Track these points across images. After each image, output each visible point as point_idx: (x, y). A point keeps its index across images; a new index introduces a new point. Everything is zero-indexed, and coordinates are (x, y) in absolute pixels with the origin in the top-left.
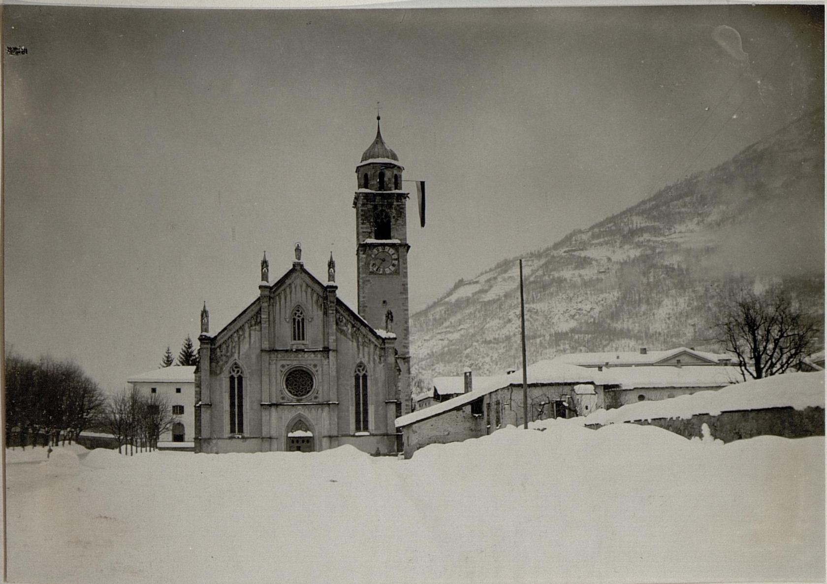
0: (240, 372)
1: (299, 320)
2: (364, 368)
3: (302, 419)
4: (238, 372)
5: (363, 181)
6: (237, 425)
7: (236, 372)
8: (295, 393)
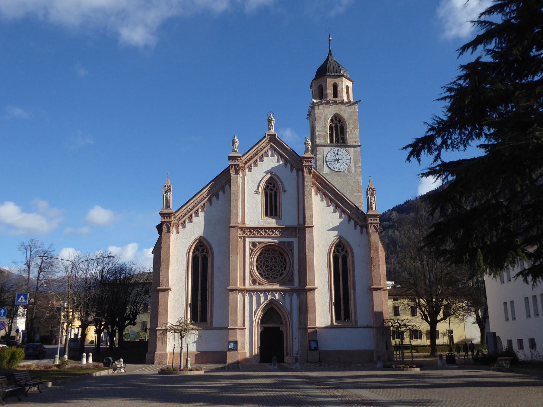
1: (271, 193)
3: (274, 307)
5: (317, 93)
6: (161, 385)
8: (267, 276)
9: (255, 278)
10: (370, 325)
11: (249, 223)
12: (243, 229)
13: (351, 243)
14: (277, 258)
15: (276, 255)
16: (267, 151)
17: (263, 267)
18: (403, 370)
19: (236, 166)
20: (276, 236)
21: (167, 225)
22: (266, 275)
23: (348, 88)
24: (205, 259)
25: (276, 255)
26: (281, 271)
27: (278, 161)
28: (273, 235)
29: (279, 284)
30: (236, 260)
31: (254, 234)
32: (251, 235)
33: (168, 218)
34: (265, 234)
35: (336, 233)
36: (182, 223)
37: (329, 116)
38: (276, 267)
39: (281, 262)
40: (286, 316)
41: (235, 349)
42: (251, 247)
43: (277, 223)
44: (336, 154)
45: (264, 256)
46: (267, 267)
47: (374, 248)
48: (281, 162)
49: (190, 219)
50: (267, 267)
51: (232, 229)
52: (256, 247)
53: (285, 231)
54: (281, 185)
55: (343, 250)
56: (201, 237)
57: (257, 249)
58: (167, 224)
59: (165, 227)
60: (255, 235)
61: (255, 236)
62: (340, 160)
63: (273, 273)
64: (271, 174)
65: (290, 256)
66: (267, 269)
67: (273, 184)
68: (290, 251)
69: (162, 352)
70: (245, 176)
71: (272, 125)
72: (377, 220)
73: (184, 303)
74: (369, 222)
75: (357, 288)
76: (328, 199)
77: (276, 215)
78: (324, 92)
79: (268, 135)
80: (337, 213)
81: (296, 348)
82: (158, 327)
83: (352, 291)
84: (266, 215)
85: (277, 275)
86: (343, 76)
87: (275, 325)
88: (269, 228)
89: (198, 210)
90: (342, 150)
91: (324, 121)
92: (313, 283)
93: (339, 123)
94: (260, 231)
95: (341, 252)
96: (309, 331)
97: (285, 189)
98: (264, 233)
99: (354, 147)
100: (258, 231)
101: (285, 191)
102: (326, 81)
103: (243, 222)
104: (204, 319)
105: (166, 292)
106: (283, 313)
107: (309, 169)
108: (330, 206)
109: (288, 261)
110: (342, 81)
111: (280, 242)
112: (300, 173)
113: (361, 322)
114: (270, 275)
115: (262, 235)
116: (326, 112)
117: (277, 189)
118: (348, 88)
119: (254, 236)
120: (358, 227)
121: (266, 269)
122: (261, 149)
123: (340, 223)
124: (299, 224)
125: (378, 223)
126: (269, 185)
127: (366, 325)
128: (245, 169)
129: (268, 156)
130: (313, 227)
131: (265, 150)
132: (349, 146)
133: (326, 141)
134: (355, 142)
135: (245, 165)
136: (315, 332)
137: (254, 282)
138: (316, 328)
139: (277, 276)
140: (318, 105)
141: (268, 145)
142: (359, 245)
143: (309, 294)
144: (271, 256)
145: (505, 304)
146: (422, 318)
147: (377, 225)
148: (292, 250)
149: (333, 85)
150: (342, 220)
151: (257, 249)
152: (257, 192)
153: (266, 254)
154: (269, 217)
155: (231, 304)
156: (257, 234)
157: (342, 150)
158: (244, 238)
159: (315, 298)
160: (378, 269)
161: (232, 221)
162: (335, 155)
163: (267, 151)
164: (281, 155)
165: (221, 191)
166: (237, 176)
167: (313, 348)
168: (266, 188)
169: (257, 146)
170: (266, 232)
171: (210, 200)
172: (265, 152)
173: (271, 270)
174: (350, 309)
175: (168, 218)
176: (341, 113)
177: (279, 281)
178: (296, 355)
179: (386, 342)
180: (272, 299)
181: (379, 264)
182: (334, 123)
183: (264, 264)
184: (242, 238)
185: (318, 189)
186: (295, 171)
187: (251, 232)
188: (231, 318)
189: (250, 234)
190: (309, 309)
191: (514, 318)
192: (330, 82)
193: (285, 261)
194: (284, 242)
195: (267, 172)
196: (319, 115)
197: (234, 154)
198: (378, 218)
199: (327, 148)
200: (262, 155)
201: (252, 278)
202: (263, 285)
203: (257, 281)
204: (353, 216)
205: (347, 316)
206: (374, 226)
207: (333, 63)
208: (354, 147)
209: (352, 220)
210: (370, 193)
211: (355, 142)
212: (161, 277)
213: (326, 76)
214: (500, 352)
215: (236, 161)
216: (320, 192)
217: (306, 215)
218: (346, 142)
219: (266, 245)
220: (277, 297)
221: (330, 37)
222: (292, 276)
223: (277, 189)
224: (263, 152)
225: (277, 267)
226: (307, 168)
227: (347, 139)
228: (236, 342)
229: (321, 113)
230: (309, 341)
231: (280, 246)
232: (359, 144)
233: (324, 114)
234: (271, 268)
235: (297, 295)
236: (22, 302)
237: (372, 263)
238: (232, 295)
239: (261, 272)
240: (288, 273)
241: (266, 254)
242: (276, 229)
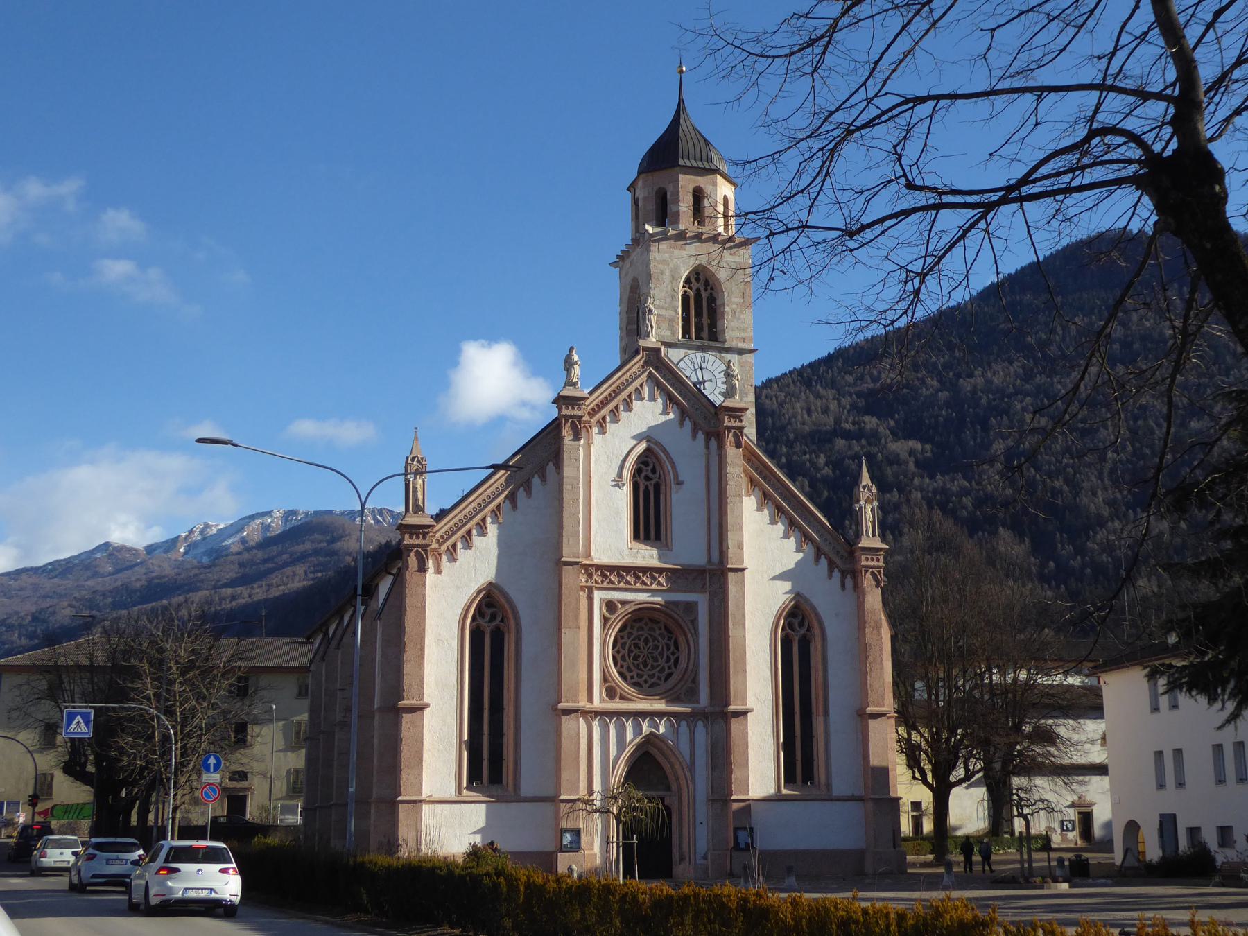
0: (499, 618)
1: (647, 487)
2: (803, 619)
3: (653, 751)
4: (493, 617)
5: (652, 206)
7: (488, 618)
8: (636, 679)
9: (613, 685)
10: (857, 794)
12: (589, 569)
13: (821, 610)
14: (660, 639)
15: (658, 632)
16: (641, 385)
17: (627, 658)
18: (1042, 888)
19: (575, 420)
20: (660, 588)
21: (417, 553)
22: (635, 677)
23: (726, 199)
24: (498, 637)
25: (658, 632)
27: (665, 412)
28: (654, 586)
29: (663, 701)
30: (573, 640)
31: (611, 582)
32: (605, 584)
33: (421, 536)
34: (635, 583)
35: (787, 585)
36: (448, 549)
37: (682, 269)
38: (656, 660)
39: (668, 649)
40: (680, 772)
41: (575, 846)
42: (605, 611)
43: (660, 558)
44: (696, 367)
45: (630, 634)
46: (636, 658)
47: (872, 624)
48: (671, 416)
49: (467, 540)
50: (636, 658)
51: (565, 568)
52: (615, 612)
53: (680, 576)
54: (670, 468)
55: (801, 624)
56: (490, 584)
57: (619, 616)
58: (417, 551)
59: (414, 558)
60: (613, 583)
61: (614, 586)
62: (706, 384)
63: (651, 673)
64: (648, 441)
65: (689, 636)
66: (636, 662)
67: (651, 465)
68: (689, 624)
70: (592, 443)
71: (651, 326)
72: (878, 560)
73: (454, 741)
74: (863, 563)
75: (831, 711)
76: (773, 507)
77: (658, 537)
78: (671, 208)
79: (645, 349)
80: (792, 540)
81: (702, 845)
82: (400, 795)
83: (821, 719)
84: (636, 537)
85: (659, 678)
86: (717, 171)
88: (645, 570)
89: (484, 520)
90: (711, 357)
91: (671, 282)
92: (744, 700)
93: (706, 290)
94: (625, 574)
95: (797, 628)
96: (735, 806)
97: (681, 479)
98: (617, 579)
99: (741, 352)
100: (620, 576)
101: (679, 483)
102: (678, 181)
103: (588, 555)
104: (496, 777)
105: (419, 713)
106: (672, 766)
107: (735, 436)
108: (776, 523)
109: (683, 646)
110: (715, 184)
111: (668, 604)
112: (713, 443)
113: (839, 789)
114: (644, 679)
115: (630, 584)
117: (659, 478)
118: (726, 199)
119: (611, 586)
120: (836, 574)
121: (634, 664)
122: (627, 380)
123: (797, 564)
124: (709, 561)
125: (880, 567)
127: (849, 793)
128: (590, 427)
129: (642, 399)
130: (743, 570)
131: (637, 384)
132: (729, 350)
133: (674, 333)
134: (744, 340)
135: (591, 418)
136: (748, 808)
137: (611, 693)
138: (749, 800)
139: (658, 681)
140: (658, 241)
141: (644, 372)
143: (735, 724)
144: (645, 633)
145: (1159, 754)
146: (914, 778)
147: (879, 572)
148: (694, 622)
149: (694, 191)
150: (801, 555)
151: (619, 616)
152: (618, 483)
153: (636, 629)
154: (643, 542)
155: (565, 742)
156: (619, 582)
157: (712, 358)
158: (591, 590)
159: (747, 732)
161: (565, 551)
162: (695, 370)
163: (641, 385)
164: (670, 399)
165: (536, 476)
166: (577, 443)
167: (742, 846)
168: (637, 475)
169: (619, 374)
170: (638, 578)
171: (512, 498)
172: (637, 388)
173: (645, 665)
174: (815, 757)
175: (421, 536)
177: (665, 692)
178: (702, 862)
179: (894, 831)
180: (651, 733)
181: (882, 660)
182: (694, 288)
183: (630, 651)
184: (584, 591)
185: (751, 481)
186: (701, 436)
187: (605, 576)
188: (565, 776)
189: (602, 582)
190: (735, 758)
191: (1180, 784)
192: (686, 183)
193: (677, 648)
194: (676, 604)
195: (639, 438)
196: (660, 266)
197: (569, 392)
198: (880, 555)
199: (676, 350)
200: (629, 396)
201: (607, 685)
202: (631, 700)
204: (825, 548)
205: (808, 776)
206: (873, 573)
207: (693, 134)
208: (741, 352)
209: (823, 556)
210: (865, 498)
211: (744, 340)
212: (405, 677)
213: (678, 169)
214: (351, 862)
215: (576, 407)
216: (757, 488)
218: (720, 337)
219: (636, 607)
220: (662, 730)
221: (681, 66)
222: (695, 681)
223: (659, 478)
224: (631, 388)
225: (660, 659)
226: (731, 434)
227: (723, 331)
228: (577, 833)
230: (736, 830)
231: (668, 611)
232: (752, 347)
233: (671, 265)
235: (705, 726)
236: (79, 731)
237: (867, 657)
238: (567, 723)
239: (624, 670)
240: (684, 674)
241: (636, 629)
242: (660, 571)
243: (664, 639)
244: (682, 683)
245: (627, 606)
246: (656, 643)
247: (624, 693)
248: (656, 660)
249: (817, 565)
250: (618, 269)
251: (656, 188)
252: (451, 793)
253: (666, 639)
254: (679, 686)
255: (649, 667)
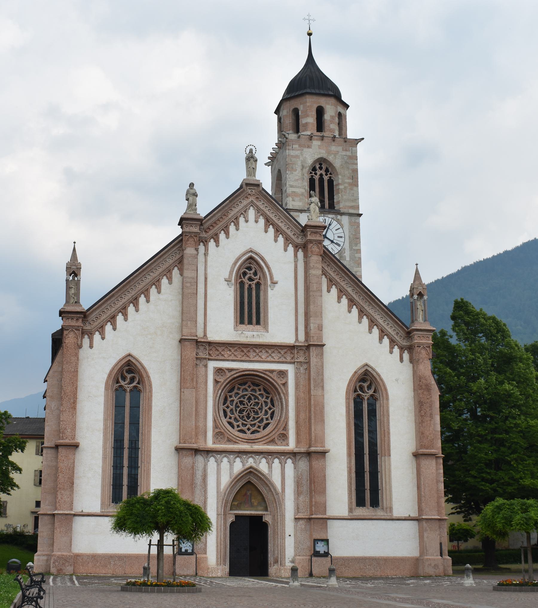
1: (250, 285)
3: (254, 480)
7: (128, 380)
11: (213, 336)
15: (240, 392)
22: (241, 425)
26: (265, 420)
46: (241, 411)
63: (253, 423)
65: (282, 395)
67: (253, 270)
69: (65, 554)
87: (253, 512)
93: (326, 175)
95: (366, 389)
97: (275, 279)
112: (300, 254)
116: (304, 155)
120: (396, 350)
124: (297, 339)
126: (247, 270)
128: (206, 241)
132: (342, 214)
139: (236, 426)
142: (397, 380)
144: (249, 393)
153: (241, 390)
160: (429, 422)
176: (331, 158)
183: (237, 407)
203: (226, 435)
209: (386, 337)
217: (312, 326)
222: (285, 428)
229: (297, 157)
234: (248, 414)
241: (241, 390)
243: (263, 398)
244: (276, 430)
245: (233, 373)
246: (257, 400)
247: (230, 438)
248: (257, 413)
249: (381, 343)
250: (270, 166)
251: (291, 109)
252: (97, 509)
253: (265, 397)
254: (274, 432)
255: (251, 419)
